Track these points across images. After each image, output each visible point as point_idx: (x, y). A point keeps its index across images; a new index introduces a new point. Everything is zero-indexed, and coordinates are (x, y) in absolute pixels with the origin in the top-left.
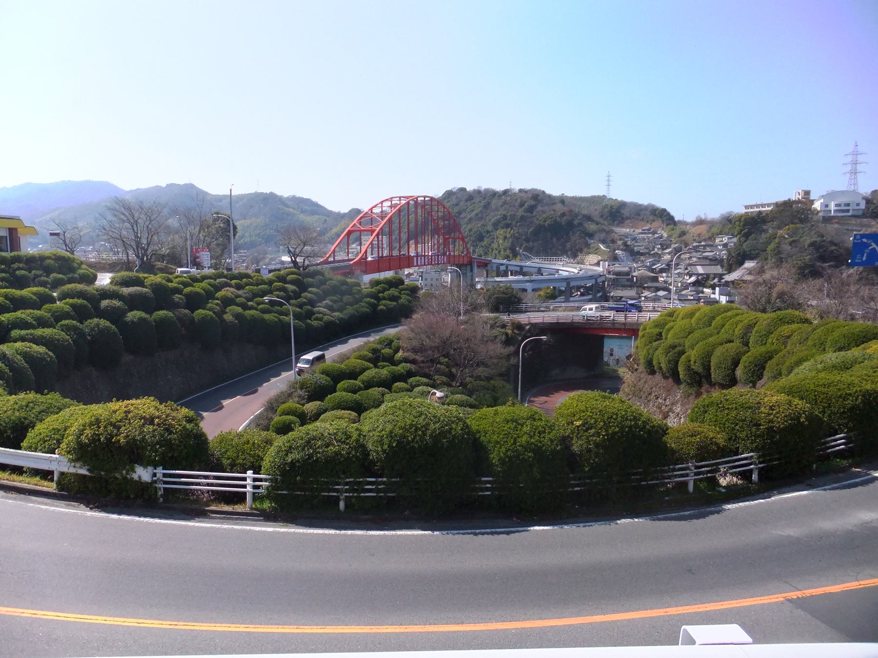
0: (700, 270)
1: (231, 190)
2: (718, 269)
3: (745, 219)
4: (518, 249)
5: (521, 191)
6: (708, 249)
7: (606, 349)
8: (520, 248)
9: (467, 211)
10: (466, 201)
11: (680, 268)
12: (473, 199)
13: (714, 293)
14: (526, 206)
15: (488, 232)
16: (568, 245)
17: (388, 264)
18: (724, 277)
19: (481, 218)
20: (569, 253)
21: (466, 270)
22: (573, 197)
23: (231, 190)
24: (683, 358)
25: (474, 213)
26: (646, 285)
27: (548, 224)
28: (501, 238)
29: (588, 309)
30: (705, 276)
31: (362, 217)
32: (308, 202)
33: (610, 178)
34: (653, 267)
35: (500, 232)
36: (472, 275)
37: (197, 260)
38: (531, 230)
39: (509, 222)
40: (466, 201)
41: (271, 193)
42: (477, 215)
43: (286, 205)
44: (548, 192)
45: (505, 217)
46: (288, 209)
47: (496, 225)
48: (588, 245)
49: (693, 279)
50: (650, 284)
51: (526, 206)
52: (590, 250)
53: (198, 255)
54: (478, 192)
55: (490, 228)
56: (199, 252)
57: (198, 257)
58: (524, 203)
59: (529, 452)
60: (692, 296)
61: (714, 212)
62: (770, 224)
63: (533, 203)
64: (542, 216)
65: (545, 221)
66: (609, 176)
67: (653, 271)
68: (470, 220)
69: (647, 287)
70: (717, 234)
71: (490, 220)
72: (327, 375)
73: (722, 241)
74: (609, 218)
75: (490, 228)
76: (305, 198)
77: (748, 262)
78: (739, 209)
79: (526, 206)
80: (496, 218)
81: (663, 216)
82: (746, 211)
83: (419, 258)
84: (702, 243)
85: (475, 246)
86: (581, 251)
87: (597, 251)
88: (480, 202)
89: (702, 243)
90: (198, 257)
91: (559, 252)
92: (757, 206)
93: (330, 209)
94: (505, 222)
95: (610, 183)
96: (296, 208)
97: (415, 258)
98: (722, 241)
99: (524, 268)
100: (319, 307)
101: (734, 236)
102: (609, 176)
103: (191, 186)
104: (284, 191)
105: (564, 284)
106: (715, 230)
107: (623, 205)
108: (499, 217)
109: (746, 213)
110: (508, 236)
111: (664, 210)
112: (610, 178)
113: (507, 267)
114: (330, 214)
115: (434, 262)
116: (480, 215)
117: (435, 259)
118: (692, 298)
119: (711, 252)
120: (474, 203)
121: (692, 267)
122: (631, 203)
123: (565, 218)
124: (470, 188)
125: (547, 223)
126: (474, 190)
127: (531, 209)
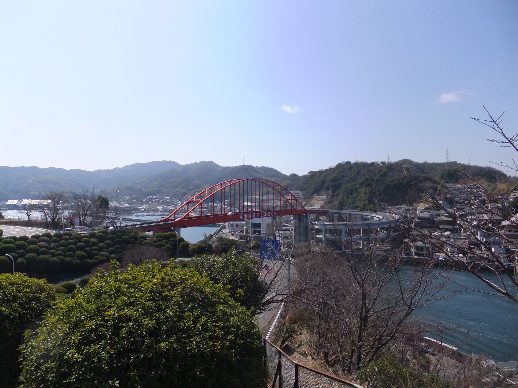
4: (374, 200)
5: (382, 163)
8: (376, 199)
9: (347, 176)
10: (348, 170)
12: (352, 169)
14: (382, 173)
15: (356, 189)
16: (407, 197)
18: (502, 222)
19: (355, 180)
20: (407, 202)
21: (303, 218)
22: (433, 163)
25: (350, 177)
27: (394, 184)
28: (363, 192)
32: (272, 170)
35: (363, 189)
36: (307, 221)
37: (72, 222)
38: (383, 188)
39: (370, 183)
40: (348, 170)
41: (250, 165)
42: (351, 178)
43: (258, 173)
44: (419, 162)
45: (367, 180)
46: (257, 174)
47: (361, 185)
48: (420, 197)
52: (422, 201)
53: (73, 220)
54: (356, 164)
55: (358, 186)
56: (73, 218)
57: (73, 221)
58: (381, 171)
63: (387, 170)
65: (392, 182)
68: (348, 181)
71: (358, 181)
74: (447, 178)
75: (358, 186)
76: (270, 167)
80: (361, 180)
84: (499, 197)
85: (348, 198)
86: (415, 201)
87: (426, 201)
88: (355, 170)
89: (499, 197)
90: (73, 221)
91: (401, 202)
94: (367, 183)
96: (263, 174)
100: (104, 251)
103: (211, 162)
104: (257, 163)
108: (363, 180)
110: (368, 191)
116: (354, 179)
118: (464, 238)
120: (352, 171)
122: (473, 166)
123: (405, 180)
124: (353, 161)
125: (393, 183)
127: (385, 175)
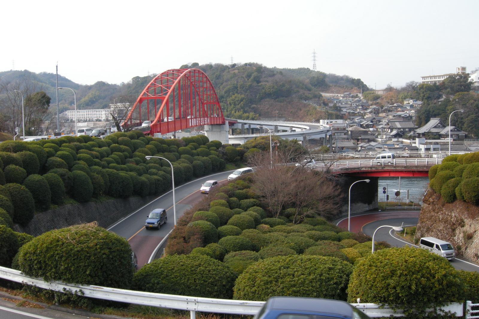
0: (398, 125)
1: (57, 67)
2: (411, 125)
3: (426, 87)
6: (399, 109)
7: (380, 190)
11: (382, 124)
13: (415, 143)
17: (169, 127)
23: (57, 67)
24: (248, 190)
26: (360, 138)
29: (381, 157)
30: (402, 130)
31: (149, 87)
33: (316, 55)
34: (361, 124)
41: (26, 71)
49: (394, 132)
50: (363, 137)
51: (252, 77)
59: (410, 284)
60: (398, 145)
61: (399, 83)
62: (444, 91)
64: (267, 84)
66: (314, 53)
67: (362, 126)
69: (361, 139)
70: (405, 99)
72: (210, 221)
73: (409, 103)
77: (433, 119)
78: (419, 80)
79: (252, 77)
81: (358, 84)
82: (424, 81)
83: (193, 120)
84: (395, 105)
92: (431, 77)
93: (76, 82)
95: (316, 58)
97: (190, 120)
98: (409, 103)
99: (251, 125)
101: (417, 99)
102: (314, 53)
105: (301, 138)
106: (401, 96)
107: (324, 75)
109: (423, 82)
111: (359, 80)
112: (316, 55)
113: (250, 126)
114: (77, 86)
115: (202, 123)
117: (202, 120)
119: (402, 111)
121: (392, 123)
122: (330, 75)
126: (21, 71)
